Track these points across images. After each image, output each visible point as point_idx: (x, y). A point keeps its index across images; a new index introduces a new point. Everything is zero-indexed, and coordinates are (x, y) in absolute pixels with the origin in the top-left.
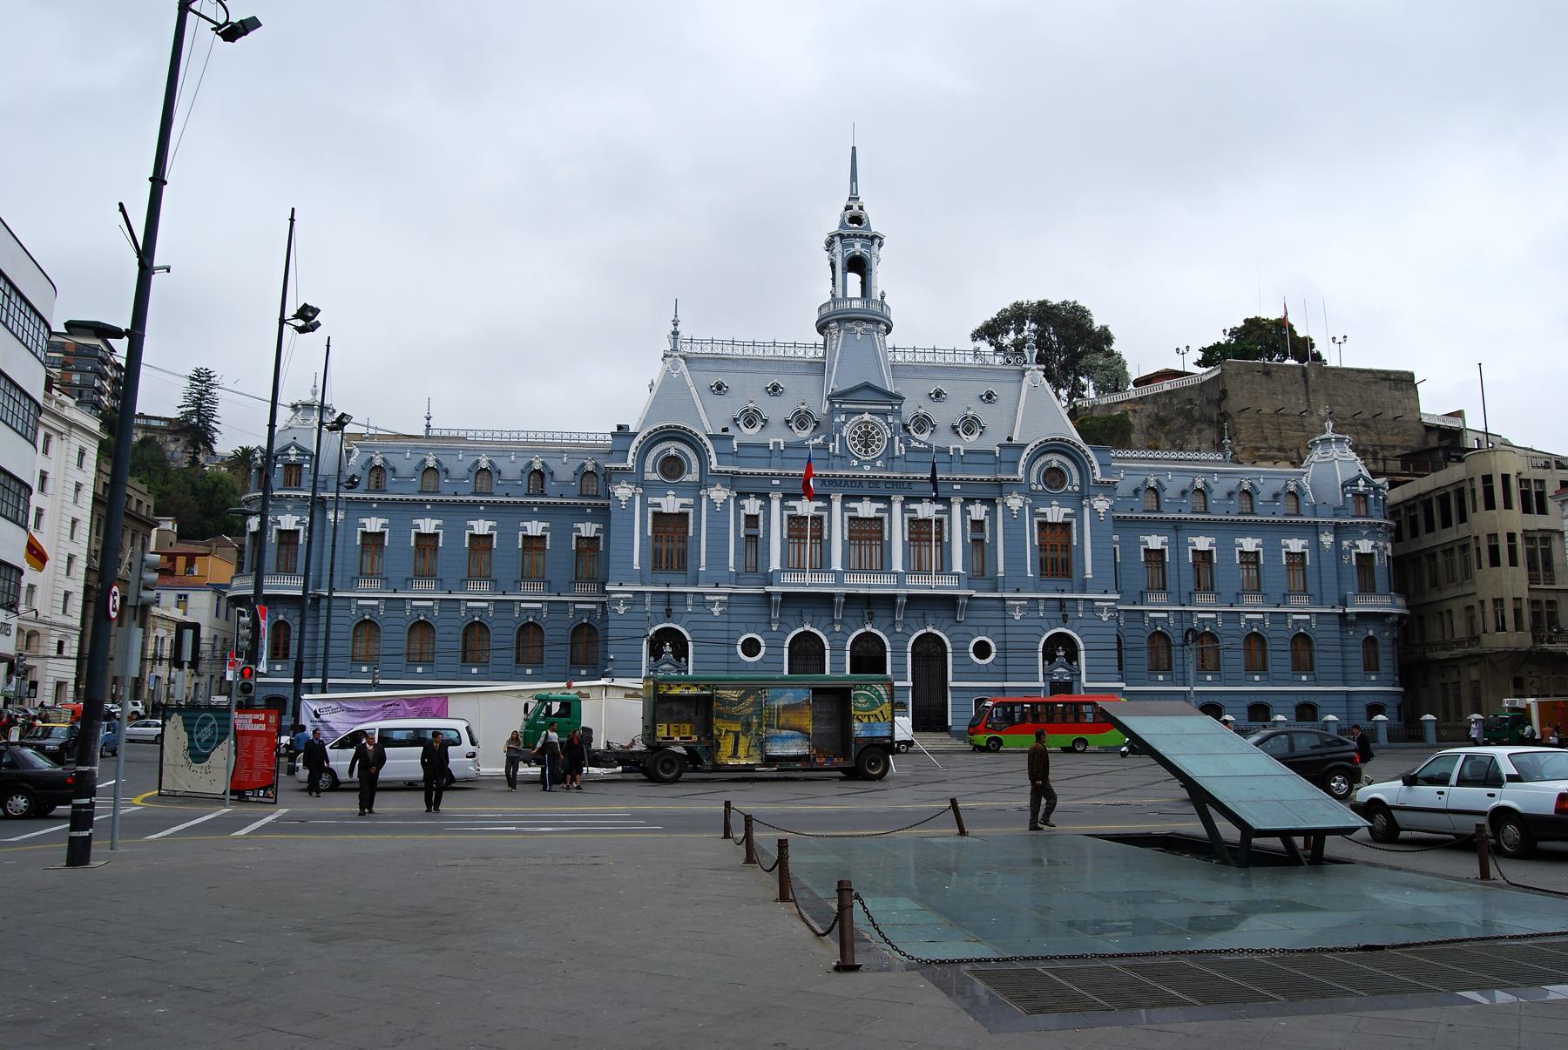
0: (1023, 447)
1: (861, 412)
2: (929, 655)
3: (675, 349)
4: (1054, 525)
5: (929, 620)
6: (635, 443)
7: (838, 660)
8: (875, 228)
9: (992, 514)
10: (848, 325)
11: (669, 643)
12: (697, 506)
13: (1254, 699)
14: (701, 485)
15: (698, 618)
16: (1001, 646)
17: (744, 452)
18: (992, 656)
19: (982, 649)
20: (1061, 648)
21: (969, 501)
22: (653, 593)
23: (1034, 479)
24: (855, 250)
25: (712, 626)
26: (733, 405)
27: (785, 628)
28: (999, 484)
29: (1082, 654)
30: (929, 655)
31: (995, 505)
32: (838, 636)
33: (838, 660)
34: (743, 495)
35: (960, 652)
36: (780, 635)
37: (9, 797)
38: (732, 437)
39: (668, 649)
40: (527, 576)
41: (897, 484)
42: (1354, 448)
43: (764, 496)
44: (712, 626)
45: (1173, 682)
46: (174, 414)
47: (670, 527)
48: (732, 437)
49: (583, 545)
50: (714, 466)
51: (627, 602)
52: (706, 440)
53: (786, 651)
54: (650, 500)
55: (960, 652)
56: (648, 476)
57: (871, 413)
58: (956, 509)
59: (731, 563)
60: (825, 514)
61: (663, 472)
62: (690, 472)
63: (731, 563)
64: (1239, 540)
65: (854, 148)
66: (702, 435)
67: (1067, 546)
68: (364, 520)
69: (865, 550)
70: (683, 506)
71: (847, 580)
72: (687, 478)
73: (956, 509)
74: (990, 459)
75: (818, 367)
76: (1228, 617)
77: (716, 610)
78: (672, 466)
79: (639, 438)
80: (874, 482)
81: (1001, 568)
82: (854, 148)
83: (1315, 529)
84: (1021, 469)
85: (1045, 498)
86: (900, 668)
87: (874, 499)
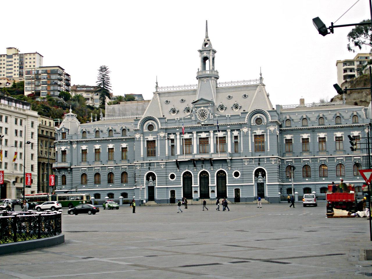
0: (247, 113)
2: (221, 177)
3: (157, 91)
4: (259, 136)
5: (204, 167)
7: (196, 179)
8: (214, 48)
9: (239, 134)
10: (202, 79)
13: (305, 186)
14: (267, 126)
15: (158, 169)
16: (242, 173)
17: (169, 122)
18: (239, 176)
20: (260, 172)
21: (232, 131)
22: (146, 163)
23: (252, 122)
24: (207, 55)
25: (162, 171)
26: (170, 107)
27: (198, 170)
28: (241, 124)
30: (221, 177)
32: (196, 172)
33: (196, 179)
35: (230, 176)
36: (227, 169)
37: (88, 211)
38: (166, 118)
42: (77, 118)
43: (174, 134)
44: (162, 171)
46: (96, 85)
48: (166, 118)
49: (321, 140)
52: (267, 113)
53: (182, 178)
54: (145, 137)
55: (230, 176)
56: (144, 131)
58: (229, 133)
59: (250, 149)
61: (256, 123)
62: (155, 129)
63: (250, 149)
64: (301, 135)
65: (207, 21)
67: (263, 142)
68: (108, 145)
70: (154, 138)
73: (229, 133)
74: (238, 117)
76: (313, 159)
77: (162, 167)
78: (151, 127)
79: (248, 114)
82: (207, 21)
83: (71, 143)
85: (148, 134)
86: (196, 181)
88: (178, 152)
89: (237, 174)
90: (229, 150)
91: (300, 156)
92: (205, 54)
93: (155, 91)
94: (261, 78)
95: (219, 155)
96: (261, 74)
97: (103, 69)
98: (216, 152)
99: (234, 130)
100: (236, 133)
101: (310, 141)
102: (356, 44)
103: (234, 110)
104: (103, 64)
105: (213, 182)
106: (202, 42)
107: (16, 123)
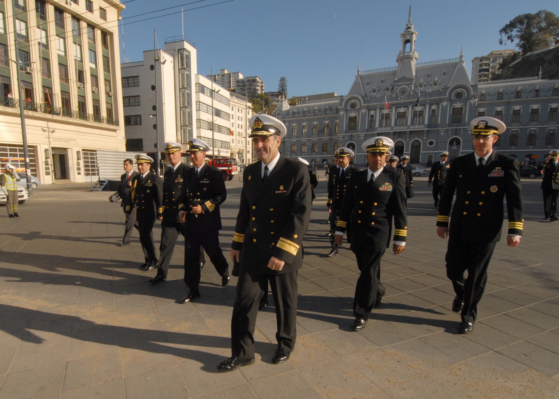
1: (402, 85)
3: (358, 75)
6: (344, 101)
11: (455, 142)
12: (359, 114)
19: (431, 143)
21: (431, 105)
23: (452, 96)
29: (461, 143)
31: (439, 106)
34: (370, 110)
39: (455, 143)
40: (532, 120)
41: (410, 103)
43: (375, 110)
45: (517, 149)
46: (277, 91)
47: (353, 120)
50: (362, 104)
51: (444, 132)
57: (405, 85)
60: (464, 107)
64: (531, 106)
66: (468, 85)
69: (401, 120)
71: (411, 127)
72: (357, 108)
73: (427, 107)
75: (394, 73)
80: (404, 103)
81: (439, 121)
84: (447, 94)
87: (404, 107)
88: (377, 125)
89: (431, 143)
90: (426, 122)
91: (546, 124)
92: (408, 37)
93: (356, 74)
94: (461, 57)
95: (417, 127)
96: (461, 53)
97: (283, 80)
98: (380, 126)
99: (432, 104)
100: (434, 107)
101: (503, 113)
102: (509, 38)
103: (433, 86)
104: (282, 76)
105: (407, 150)
106: (405, 27)
107: (238, 111)
